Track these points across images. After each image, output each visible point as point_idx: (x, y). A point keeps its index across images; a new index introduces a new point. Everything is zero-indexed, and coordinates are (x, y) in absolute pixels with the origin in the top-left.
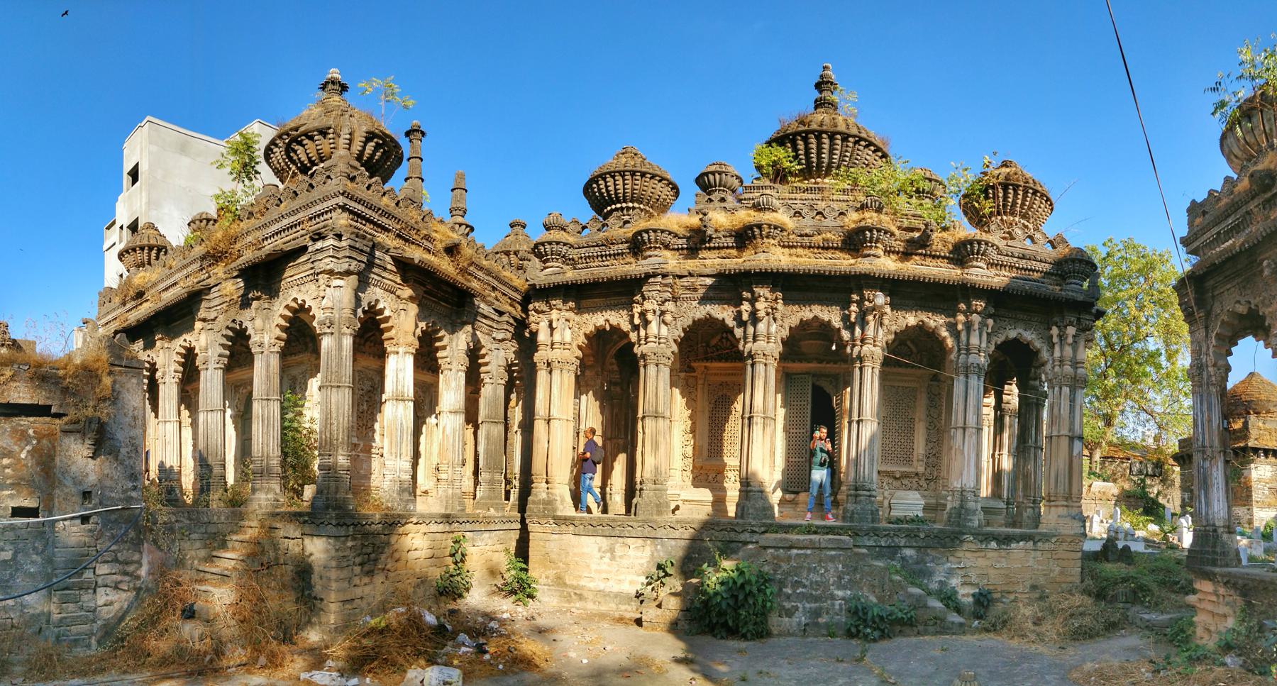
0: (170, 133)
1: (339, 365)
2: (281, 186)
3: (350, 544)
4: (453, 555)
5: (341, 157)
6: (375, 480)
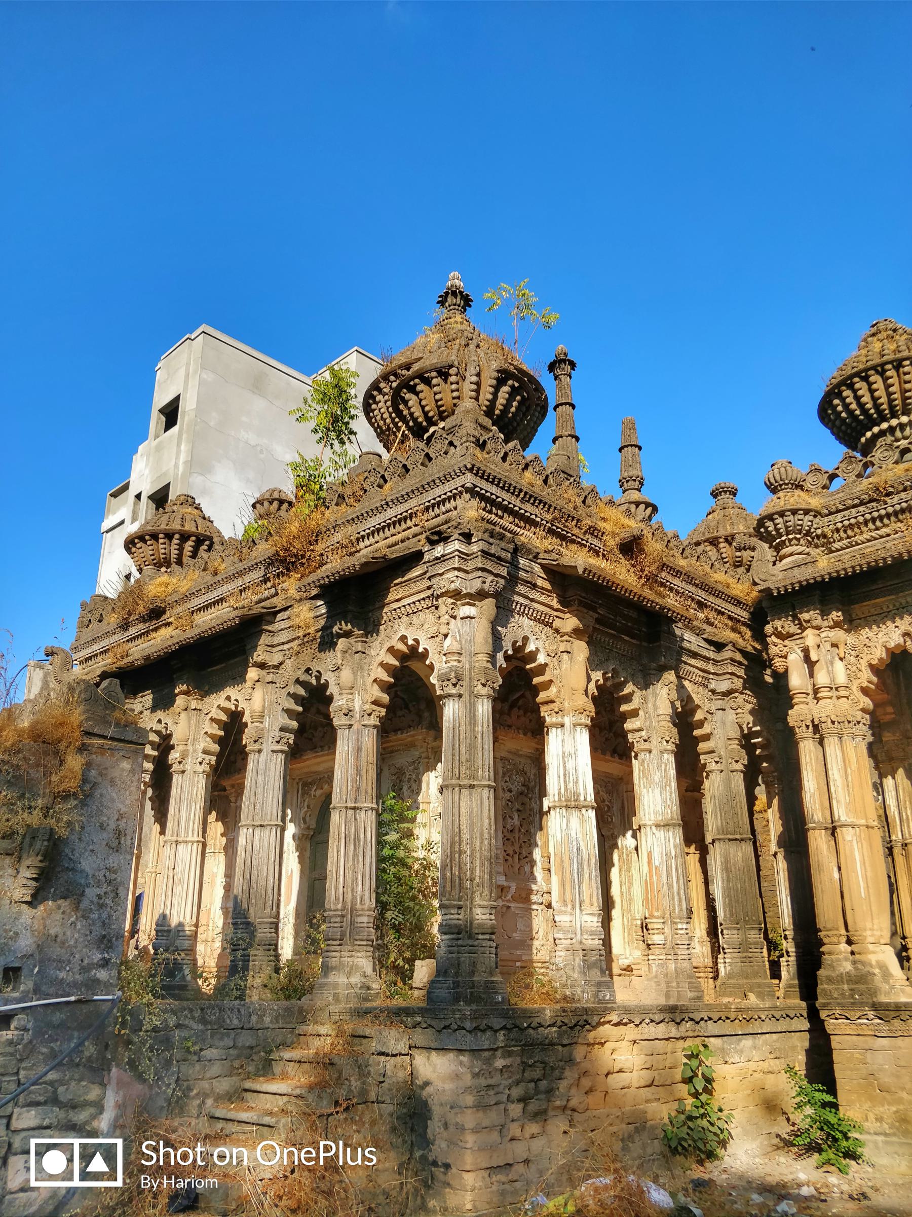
0: (237, 357)
1: (472, 748)
2: (386, 456)
3: (499, 1063)
4: (688, 1081)
5: (468, 412)
6: (540, 950)
